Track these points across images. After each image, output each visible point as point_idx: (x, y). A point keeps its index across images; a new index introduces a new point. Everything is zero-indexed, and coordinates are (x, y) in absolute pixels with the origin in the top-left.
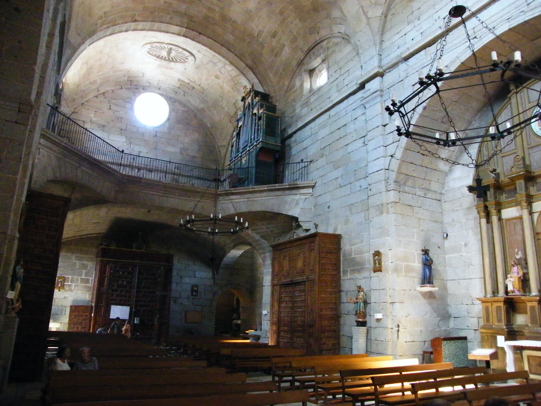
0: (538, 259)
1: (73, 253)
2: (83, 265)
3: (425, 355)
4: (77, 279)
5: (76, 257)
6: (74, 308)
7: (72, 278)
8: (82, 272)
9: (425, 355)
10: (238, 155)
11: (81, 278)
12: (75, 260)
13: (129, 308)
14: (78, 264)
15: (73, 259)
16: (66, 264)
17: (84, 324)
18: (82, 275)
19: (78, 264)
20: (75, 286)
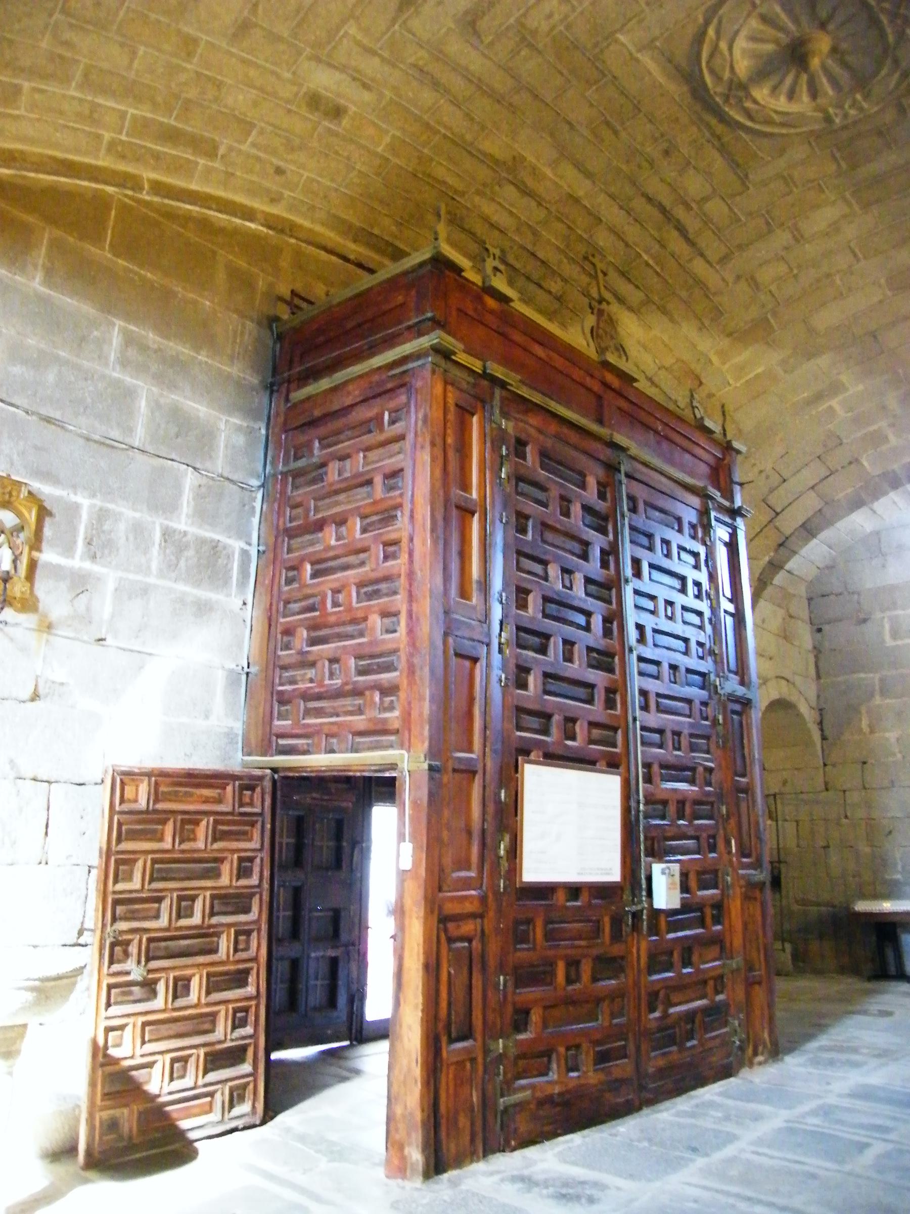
0: (447, 1078)
1: (108, 308)
2: (176, 415)
3: (121, 867)
4: (138, 529)
5: (129, 340)
6: (142, 796)
7: (102, 515)
8: (178, 487)
9: (121, 867)
10: (796, 186)
11: (167, 534)
12: (124, 363)
13: (615, 876)
14: (143, 404)
15: (37, 280)
16: (51, 377)
17: (224, 944)
18: (170, 507)
19: (143, 404)
20: (124, 592)
